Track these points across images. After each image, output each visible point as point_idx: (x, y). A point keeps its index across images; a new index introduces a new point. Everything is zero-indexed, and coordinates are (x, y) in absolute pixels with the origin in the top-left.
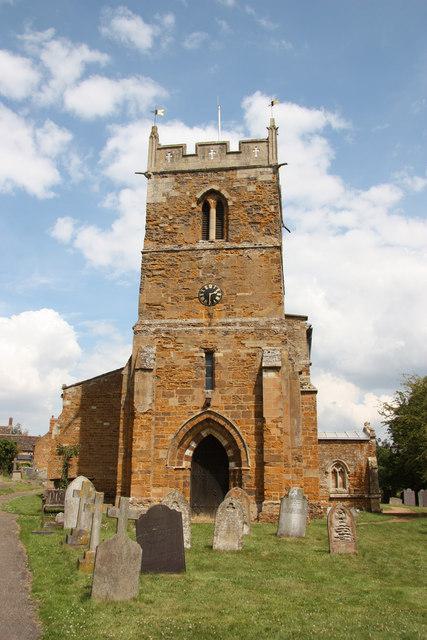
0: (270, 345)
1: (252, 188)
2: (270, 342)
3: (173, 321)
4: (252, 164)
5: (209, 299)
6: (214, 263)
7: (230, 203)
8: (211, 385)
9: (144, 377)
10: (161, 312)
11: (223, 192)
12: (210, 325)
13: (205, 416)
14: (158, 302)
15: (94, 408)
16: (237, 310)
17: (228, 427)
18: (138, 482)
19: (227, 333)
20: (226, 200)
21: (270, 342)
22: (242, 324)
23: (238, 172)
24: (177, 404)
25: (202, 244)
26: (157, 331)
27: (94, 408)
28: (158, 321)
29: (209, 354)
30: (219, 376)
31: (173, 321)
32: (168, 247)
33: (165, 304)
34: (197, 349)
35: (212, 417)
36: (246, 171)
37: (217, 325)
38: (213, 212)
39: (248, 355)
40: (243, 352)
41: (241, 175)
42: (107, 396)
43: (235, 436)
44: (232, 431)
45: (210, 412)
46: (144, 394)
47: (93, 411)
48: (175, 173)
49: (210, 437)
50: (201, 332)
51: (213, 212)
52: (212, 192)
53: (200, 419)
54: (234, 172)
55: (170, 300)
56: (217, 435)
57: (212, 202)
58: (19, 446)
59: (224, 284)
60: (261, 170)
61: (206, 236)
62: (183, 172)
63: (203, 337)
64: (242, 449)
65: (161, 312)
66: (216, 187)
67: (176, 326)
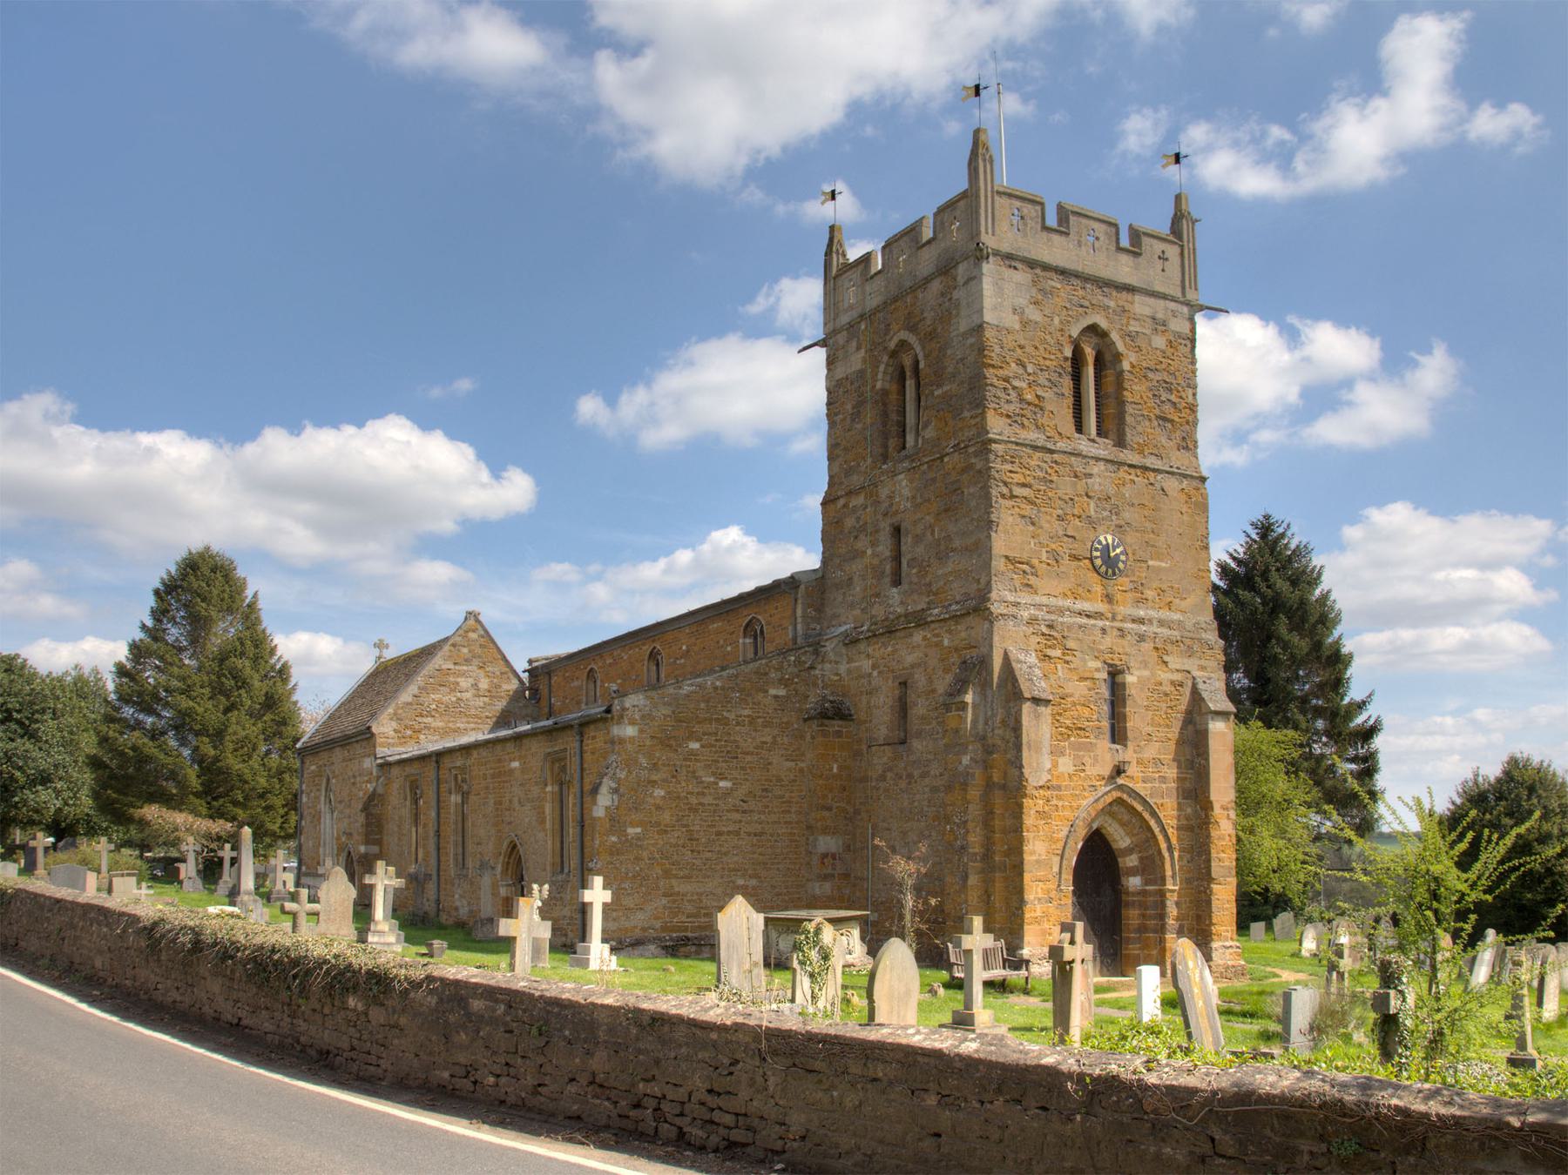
0: (1202, 668)
1: (1160, 342)
2: (1203, 662)
3: (1053, 601)
4: (1159, 288)
5: (1108, 566)
6: (1111, 492)
7: (1126, 366)
8: (1118, 734)
9: (1038, 716)
10: (1033, 580)
11: (1114, 336)
12: (1114, 619)
13: (1116, 794)
14: (1025, 557)
15: (695, 745)
16: (1150, 594)
17: (1147, 816)
18: (1037, 921)
19: (1142, 638)
20: (1118, 357)
21: (1203, 662)
22: (1161, 623)
23: (1137, 298)
24: (1071, 769)
25: (1083, 445)
26: (1032, 621)
27: (695, 745)
29: (1115, 676)
30: (1137, 721)
31: (1053, 601)
32: (1031, 435)
33: (1035, 562)
34: (1099, 664)
35: (1125, 796)
36: (1152, 301)
38: (1090, 372)
39: (1172, 683)
40: (1165, 676)
41: (1142, 306)
42: (724, 721)
43: (1157, 830)
44: (1152, 823)
45: (1121, 788)
46: (1038, 750)
47: (692, 753)
48: (1032, 264)
50: (1104, 630)
51: (1090, 372)
52: (1093, 329)
53: (1109, 799)
54: (1129, 297)
55: (1044, 556)
57: (1089, 353)
58: (61, 772)
59: (1129, 539)
60: (1172, 305)
61: (1079, 428)
62: (1046, 267)
63: (1108, 641)
64: (1166, 855)
65: (1033, 580)
66: (1104, 324)
67: (1061, 611)
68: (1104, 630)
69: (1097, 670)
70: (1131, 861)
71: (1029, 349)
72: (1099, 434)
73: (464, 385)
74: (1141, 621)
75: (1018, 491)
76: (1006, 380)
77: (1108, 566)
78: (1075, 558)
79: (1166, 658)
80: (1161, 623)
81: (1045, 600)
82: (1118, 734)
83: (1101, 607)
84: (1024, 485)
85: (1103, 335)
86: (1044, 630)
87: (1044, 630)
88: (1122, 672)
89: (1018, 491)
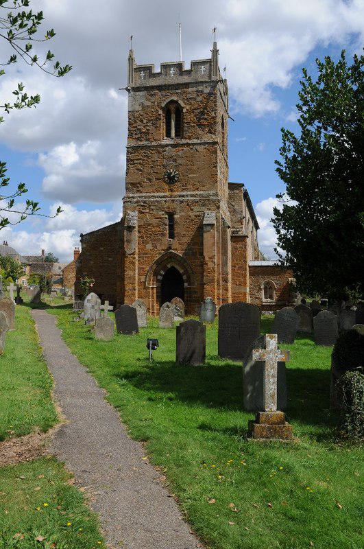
15: (102, 249)
19: (182, 202)
22: (192, 196)
25: (166, 141)
26: (137, 202)
27: (102, 249)
28: (138, 195)
29: (171, 216)
30: (177, 229)
32: (144, 143)
37: (176, 197)
49: (173, 267)
50: (165, 201)
51: (173, 116)
52: (172, 101)
56: (178, 268)
57: (172, 108)
61: (168, 135)
66: (175, 98)
68: (165, 201)
69: (163, 214)
70: (185, 277)
71: (145, 116)
72: (176, 136)
73: (244, 139)
74: (183, 196)
75: (135, 162)
76: (136, 127)
77: (171, 180)
78: (157, 179)
79: (192, 207)
80: (192, 196)
81: (144, 194)
82: (172, 236)
83: (167, 194)
84: (138, 160)
85: (176, 102)
86: (142, 204)
87: (142, 204)
88: (174, 214)
89: (135, 162)
